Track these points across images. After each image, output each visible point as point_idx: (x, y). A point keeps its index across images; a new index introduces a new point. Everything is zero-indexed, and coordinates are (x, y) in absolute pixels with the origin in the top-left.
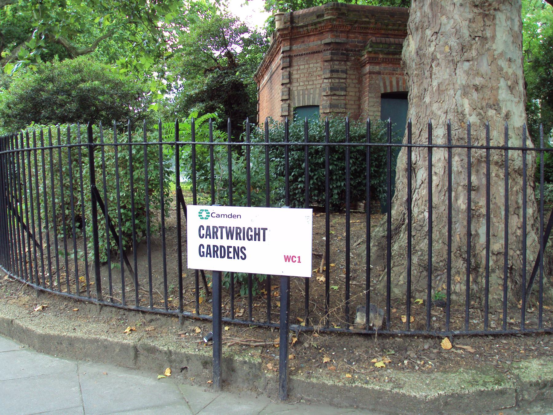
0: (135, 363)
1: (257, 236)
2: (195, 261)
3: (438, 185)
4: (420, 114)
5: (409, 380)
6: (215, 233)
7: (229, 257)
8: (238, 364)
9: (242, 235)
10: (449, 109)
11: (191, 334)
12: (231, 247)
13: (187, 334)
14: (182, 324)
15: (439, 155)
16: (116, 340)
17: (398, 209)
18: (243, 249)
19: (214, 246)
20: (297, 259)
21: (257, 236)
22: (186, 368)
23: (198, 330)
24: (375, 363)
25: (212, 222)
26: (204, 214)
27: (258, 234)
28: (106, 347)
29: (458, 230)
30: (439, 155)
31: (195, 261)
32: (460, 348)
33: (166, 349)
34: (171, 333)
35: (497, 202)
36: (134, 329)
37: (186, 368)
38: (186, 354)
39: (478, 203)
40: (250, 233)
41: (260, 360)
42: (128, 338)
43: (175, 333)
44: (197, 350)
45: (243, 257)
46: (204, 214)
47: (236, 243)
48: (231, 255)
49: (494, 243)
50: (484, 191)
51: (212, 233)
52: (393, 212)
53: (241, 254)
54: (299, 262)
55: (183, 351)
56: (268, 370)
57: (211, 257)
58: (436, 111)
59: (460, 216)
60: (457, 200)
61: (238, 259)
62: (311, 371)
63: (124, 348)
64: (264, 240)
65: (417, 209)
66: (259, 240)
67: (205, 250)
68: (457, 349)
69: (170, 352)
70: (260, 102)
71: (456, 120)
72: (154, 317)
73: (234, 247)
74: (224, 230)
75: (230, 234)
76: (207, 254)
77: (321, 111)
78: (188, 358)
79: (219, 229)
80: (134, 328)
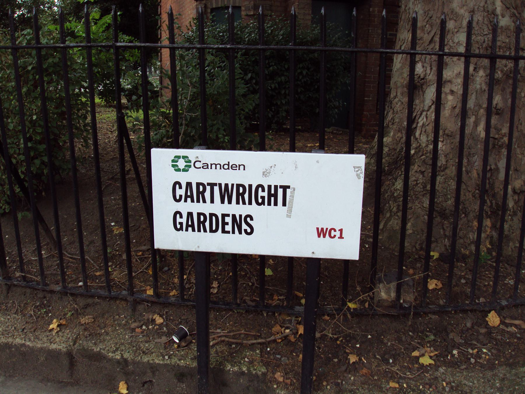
0: (72, 375)
1: (273, 199)
2: (167, 237)
3: (455, 108)
4: (431, 13)
5: (474, 383)
6: (201, 194)
7: (224, 231)
8: (231, 376)
9: (246, 196)
10: (476, 8)
11: (150, 327)
12: (228, 215)
13: (144, 327)
14: (134, 310)
15: (454, 70)
16: (39, 346)
17: (394, 135)
18: (248, 219)
19: (199, 214)
20: (338, 234)
21: (273, 199)
22: (151, 381)
23: (159, 320)
24: (417, 358)
25: (195, 176)
26: (181, 164)
27: (274, 195)
28: (24, 354)
29: (476, 164)
30: (454, 70)
31: (167, 237)
32: (511, 325)
33: (118, 357)
34: (119, 325)
35: (522, 128)
36: (64, 323)
37: (151, 381)
38: (150, 364)
39: (501, 130)
40: (261, 194)
41: (264, 370)
42: (56, 337)
43: (125, 325)
44: (167, 357)
45: (249, 230)
46: (181, 164)
47: (235, 209)
48: (228, 228)
49: (516, 179)
50: (507, 116)
51: (197, 192)
52: (386, 140)
53: (244, 226)
54: (341, 237)
55: (145, 359)
56: (278, 383)
57: (194, 230)
58: (457, 10)
59: (479, 146)
60: (477, 126)
61: (240, 233)
62: (339, 381)
63: (53, 355)
64: (284, 204)
65: (425, 137)
66: (276, 204)
67: (184, 220)
68: (507, 325)
69: (126, 360)
70: (162, 4)
71: (486, 22)
72: (90, 301)
73: (234, 216)
74: (216, 189)
75: (226, 194)
76: (188, 226)
77: (243, 13)
78: (154, 368)
79: (208, 188)
80: (63, 322)
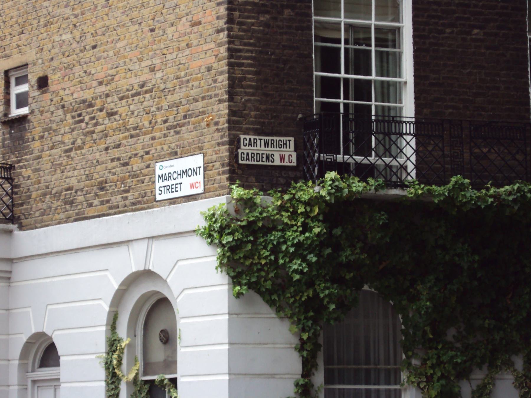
9: (275, 144)
19: (252, 154)
31: (292, 139)
53: (270, 159)
73: (267, 154)
